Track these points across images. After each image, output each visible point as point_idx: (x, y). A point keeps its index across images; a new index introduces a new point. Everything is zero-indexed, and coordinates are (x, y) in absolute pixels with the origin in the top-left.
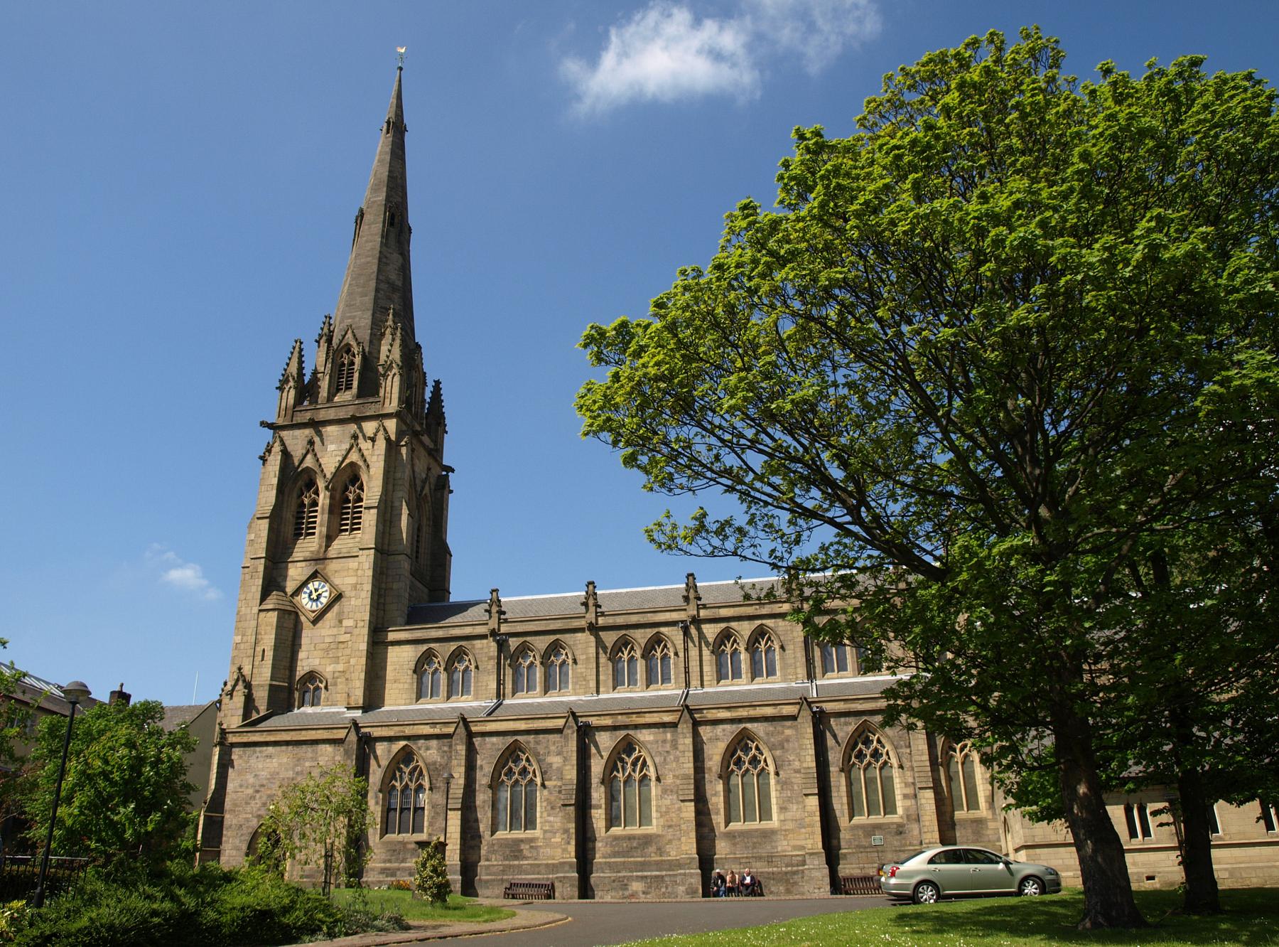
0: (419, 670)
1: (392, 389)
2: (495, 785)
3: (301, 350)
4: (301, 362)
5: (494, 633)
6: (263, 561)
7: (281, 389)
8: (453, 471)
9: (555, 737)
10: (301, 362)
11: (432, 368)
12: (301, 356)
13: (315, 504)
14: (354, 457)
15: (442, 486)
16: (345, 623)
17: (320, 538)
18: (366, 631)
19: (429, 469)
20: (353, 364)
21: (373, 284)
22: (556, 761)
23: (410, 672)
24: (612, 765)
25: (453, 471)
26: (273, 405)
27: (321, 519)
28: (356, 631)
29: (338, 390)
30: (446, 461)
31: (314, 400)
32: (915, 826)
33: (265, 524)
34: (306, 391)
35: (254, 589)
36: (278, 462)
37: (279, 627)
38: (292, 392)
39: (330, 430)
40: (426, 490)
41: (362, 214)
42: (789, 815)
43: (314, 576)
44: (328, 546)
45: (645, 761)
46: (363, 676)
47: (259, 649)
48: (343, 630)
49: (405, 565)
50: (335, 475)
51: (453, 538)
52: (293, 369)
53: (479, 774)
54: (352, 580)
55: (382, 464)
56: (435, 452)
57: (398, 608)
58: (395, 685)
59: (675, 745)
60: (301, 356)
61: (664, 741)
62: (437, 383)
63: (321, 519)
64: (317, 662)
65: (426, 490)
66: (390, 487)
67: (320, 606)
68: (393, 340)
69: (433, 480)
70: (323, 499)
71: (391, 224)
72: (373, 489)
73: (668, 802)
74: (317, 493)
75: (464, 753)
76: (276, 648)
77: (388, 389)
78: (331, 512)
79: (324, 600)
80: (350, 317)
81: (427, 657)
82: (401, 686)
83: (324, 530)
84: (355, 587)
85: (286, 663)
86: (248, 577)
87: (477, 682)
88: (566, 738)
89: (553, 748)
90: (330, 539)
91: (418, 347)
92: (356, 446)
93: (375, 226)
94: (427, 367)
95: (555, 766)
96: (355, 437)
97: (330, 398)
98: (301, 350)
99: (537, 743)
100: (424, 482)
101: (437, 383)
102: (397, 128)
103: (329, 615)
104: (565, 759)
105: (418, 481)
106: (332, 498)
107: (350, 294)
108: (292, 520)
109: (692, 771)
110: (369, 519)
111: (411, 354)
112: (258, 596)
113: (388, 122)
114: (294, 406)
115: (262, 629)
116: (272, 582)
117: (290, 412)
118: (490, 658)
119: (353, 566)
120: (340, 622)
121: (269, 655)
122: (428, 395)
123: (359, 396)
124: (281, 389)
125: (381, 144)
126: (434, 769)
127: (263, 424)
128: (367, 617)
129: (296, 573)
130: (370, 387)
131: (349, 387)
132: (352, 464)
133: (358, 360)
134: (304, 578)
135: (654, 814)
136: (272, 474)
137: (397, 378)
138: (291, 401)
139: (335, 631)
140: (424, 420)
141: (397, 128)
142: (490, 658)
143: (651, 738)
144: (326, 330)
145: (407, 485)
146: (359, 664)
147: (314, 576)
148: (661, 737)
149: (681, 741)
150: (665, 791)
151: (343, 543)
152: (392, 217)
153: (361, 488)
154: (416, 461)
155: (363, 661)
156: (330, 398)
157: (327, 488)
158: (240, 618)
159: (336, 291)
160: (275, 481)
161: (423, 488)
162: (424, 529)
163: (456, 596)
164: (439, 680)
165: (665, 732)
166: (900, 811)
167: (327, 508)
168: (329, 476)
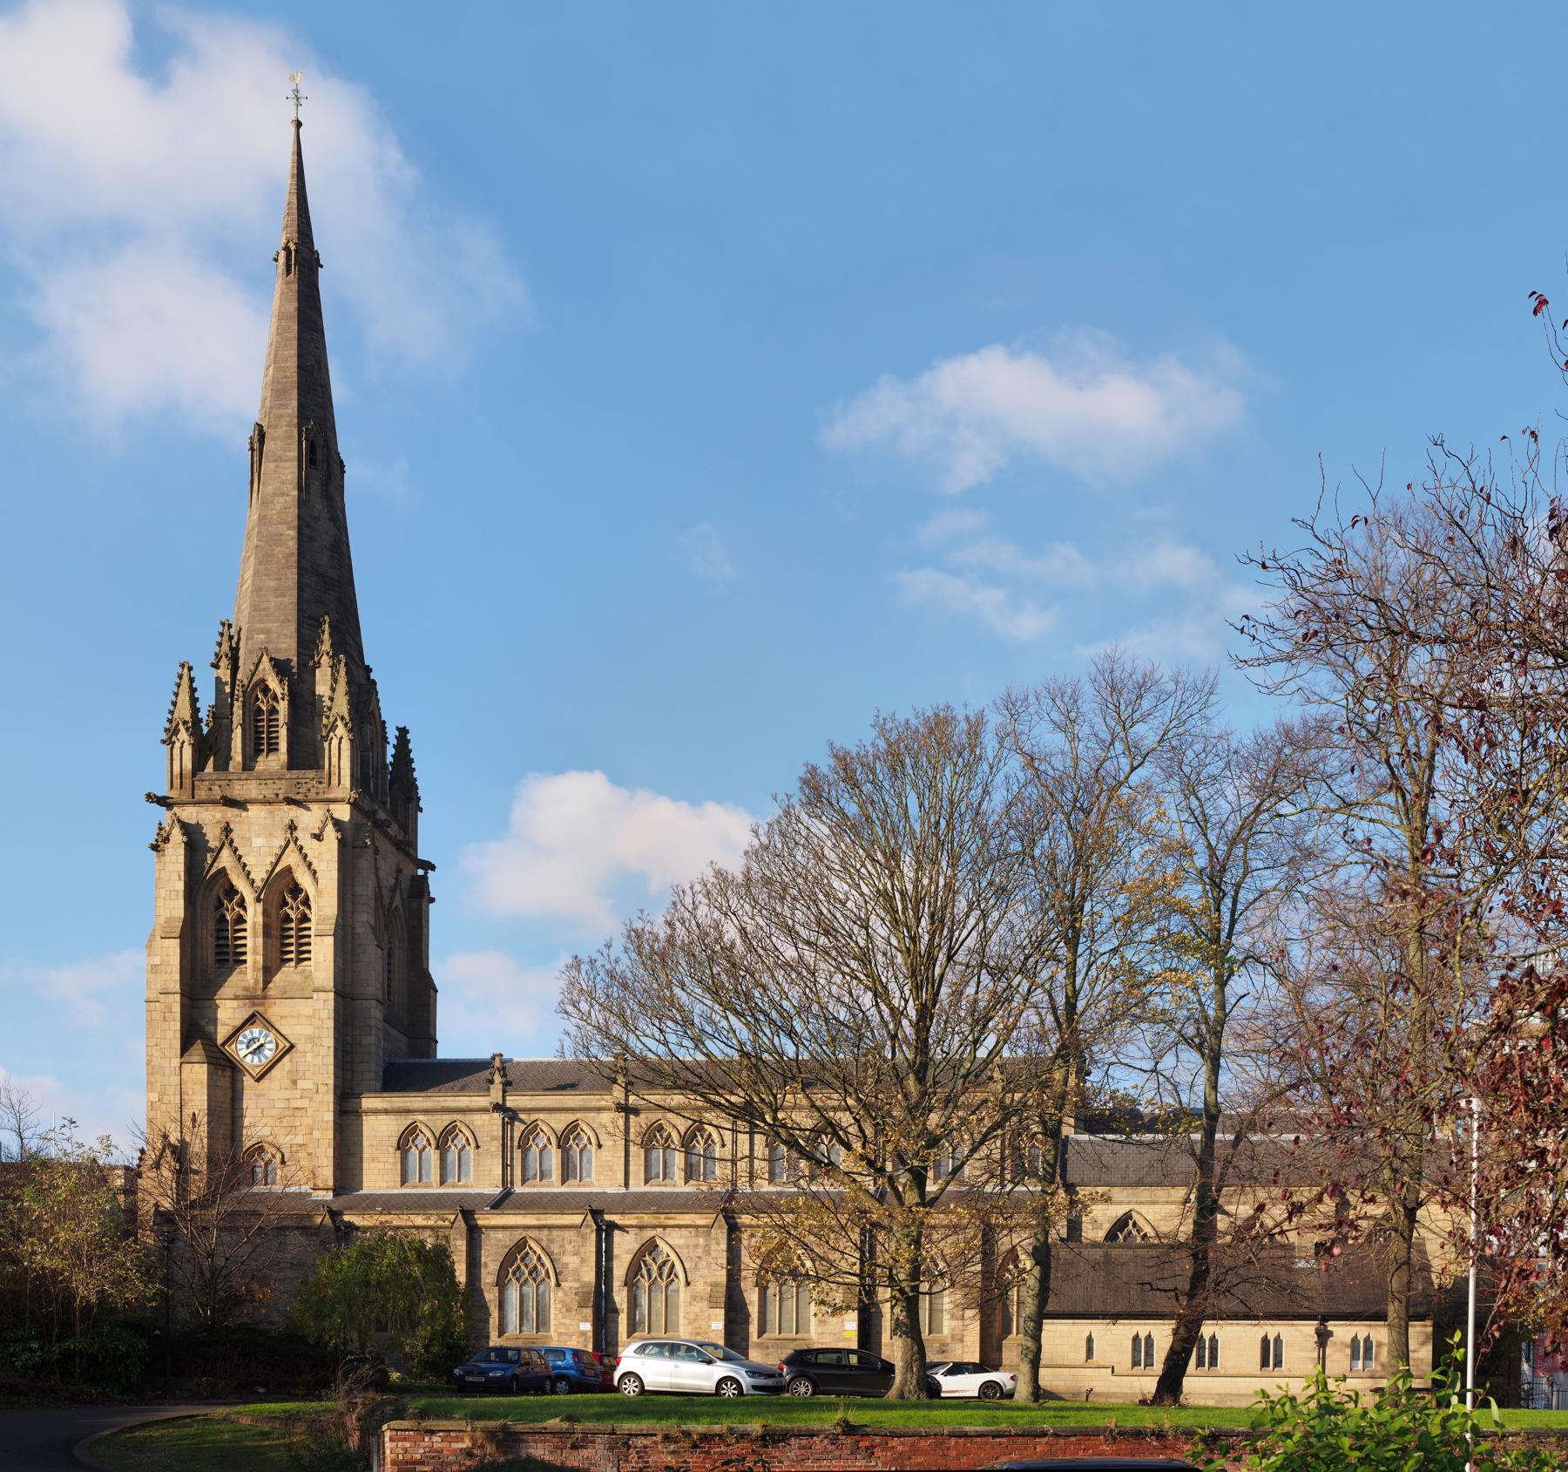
0: (403, 1145)
1: (339, 751)
2: (501, 1284)
3: (192, 680)
4: (194, 700)
5: (498, 1108)
6: (178, 997)
7: (169, 742)
8: (433, 868)
9: (570, 1234)
10: (194, 700)
11: (392, 713)
12: (193, 690)
13: (241, 920)
15: (419, 894)
16: (301, 1084)
17: (255, 969)
18: (330, 1097)
19: (399, 871)
20: (273, 711)
21: (293, 575)
22: (571, 1261)
23: (392, 1150)
24: (635, 1269)
25: (433, 868)
26: (160, 765)
27: (253, 944)
28: (317, 1098)
29: (258, 752)
30: (422, 854)
31: (223, 765)
32: (959, 1346)
33: (174, 946)
34: (209, 747)
35: (170, 1034)
36: (182, 859)
37: (212, 1086)
38: (188, 752)
40: (397, 901)
41: (261, 434)
42: (827, 1328)
43: (250, 1021)
44: (266, 982)
45: (673, 1265)
46: (331, 1152)
47: (188, 1112)
48: (298, 1093)
49: (375, 1013)
50: (266, 882)
51: (439, 968)
52: (184, 711)
53: (616, 1264)
54: (308, 1030)
55: (335, 874)
56: (407, 845)
57: (370, 1069)
58: (373, 1165)
59: (707, 1251)
60: (193, 690)
61: (696, 1246)
62: (403, 732)
63: (253, 944)
64: (267, 1131)
65: (397, 901)
66: (349, 904)
67: (247, 1033)
68: (335, 681)
69: (405, 883)
70: (254, 915)
71: (312, 462)
72: (324, 901)
73: (697, 1309)
74: (242, 904)
75: (464, 1248)
76: (211, 1112)
77: (335, 760)
78: (266, 934)
79: (269, 1053)
80: (262, 631)
81: (410, 1133)
82: (381, 1166)
83: (260, 958)
84: (311, 1039)
85: (224, 1131)
86: (156, 1016)
87: (477, 1165)
88: (584, 1237)
89: (569, 1248)
90: (269, 972)
91: (374, 682)
92: (287, 837)
93: (284, 470)
94: (385, 715)
95: (571, 1266)
97: (248, 765)
98: (192, 680)
99: (551, 1241)
100: (393, 890)
101: (403, 732)
102: (303, 261)
103: (275, 1072)
104: (583, 1260)
105: (385, 892)
106: (265, 913)
107: (257, 589)
108: (211, 942)
109: (724, 1279)
110: (323, 951)
111: (363, 692)
112: (177, 1044)
113: (287, 249)
114: (194, 774)
115: (188, 1087)
116: (196, 1030)
117: (188, 783)
118: (493, 1138)
119: (306, 1011)
120: (294, 1082)
121: (203, 1119)
122: (390, 751)
123: (292, 765)
124: (169, 742)
125: (278, 292)
127: (150, 798)
128: (331, 1082)
129: (228, 1013)
130: (306, 755)
131: (273, 748)
132: (288, 870)
133: (283, 707)
134: (238, 1023)
135: (682, 1321)
136: (175, 876)
137: (346, 745)
138: (188, 764)
139: (288, 1094)
140: (388, 792)
142: (493, 1138)
143: (682, 1242)
144: (225, 647)
145: (372, 903)
146: (324, 1138)
147: (250, 1021)
148: (693, 1241)
149: (714, 1247)
150: (694, 1298)
151: (287, 975)
152: (312, 448)
153: (306, 902)
154: (381, 863)
155: (330, 1134)
156: (248, 765)
157: (258, 900)
158: (152, 1067)
159: (234, 582)
160: (180, 886)
161: (392, 898)
162: (397, 953)
163: (448, 1048)
164: (429, 1161)
165: (697, 1236)
166: (946, 1331)
167: (260, 929)
168: (259, 883)
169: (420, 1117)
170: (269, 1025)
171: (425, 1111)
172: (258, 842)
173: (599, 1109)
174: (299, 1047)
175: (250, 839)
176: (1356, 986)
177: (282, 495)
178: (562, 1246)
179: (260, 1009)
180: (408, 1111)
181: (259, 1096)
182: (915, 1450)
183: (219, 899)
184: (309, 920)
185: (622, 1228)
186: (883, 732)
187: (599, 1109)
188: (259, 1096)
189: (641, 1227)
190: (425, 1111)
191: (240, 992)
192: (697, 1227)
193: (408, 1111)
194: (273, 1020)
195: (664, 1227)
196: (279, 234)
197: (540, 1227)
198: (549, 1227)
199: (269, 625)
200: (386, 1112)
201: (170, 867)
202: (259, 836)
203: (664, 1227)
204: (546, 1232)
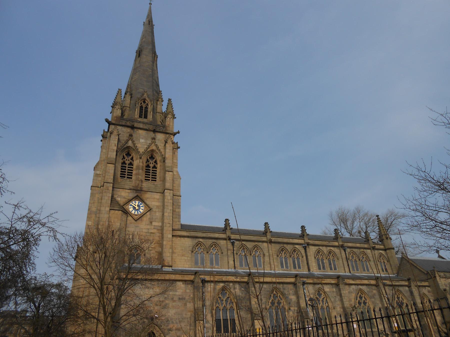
14: (153, 147)
16: (154, 224)
20: (146, 108)
39: (140, 132)
82: (186, 258)
96: (154, 139)
102: (149, 23)
120: (151, 223)
136: (113, 145)
139: (149, 227)
141: (149, 23)
169: (201, 240)
170: (142, 200)
171: (203, 238)
173: (263, 242)
174: (154, 210)
175: (139, 139)
176: (282, 250)
178: (288, 291)
179: (139, 194)
180: (197, 237)
181: (137, 226)
183: (124, 156)
184: (156, 168)
188: (137, 226)
190: (203, 238)
192: (332, 284)
193: (197, 237)
194: (144, 199)
196: (144, 19)
197: (279, 283)
198: (283, 283)
200: (188, 237)
201: (112, 141)
202: (142, 139)
204: (281, 285)
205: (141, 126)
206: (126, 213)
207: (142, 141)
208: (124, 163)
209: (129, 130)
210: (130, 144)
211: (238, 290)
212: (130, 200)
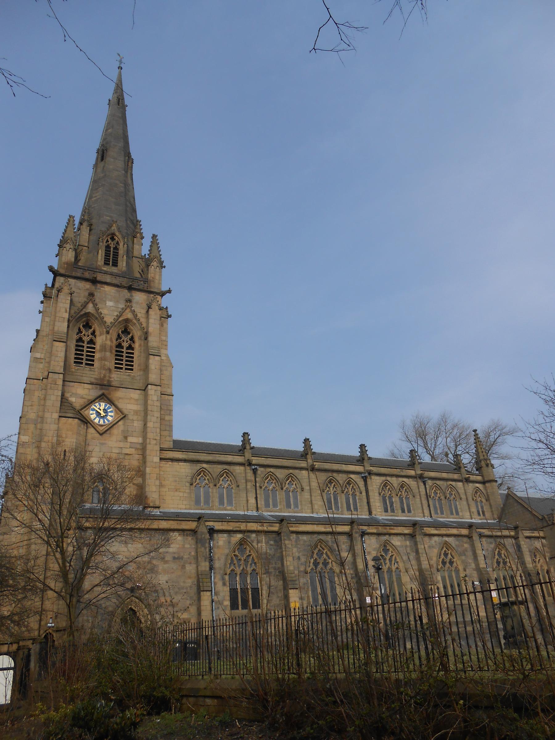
14: (129, 316)
16: (130, 439)
48: (128, 445)
82: (181, 494)
96: (129, 301)
102: (119, 103)
120: (126, 438)
126: (266, 559)
136: (64, 310)
139: (122, 445)
141: (119, 103)
165: (405, 540)
170: (111, 402)
171: (208, 462)
172: (110, 304)
173: (301, 469)
174: (130, 417)
175: (105, 301)
177: (117, 171)
179: (105, 392)
180: (198, 461)
181: (102, 444)
182: (448, 628)
184: (133, 349)
185: (368, 534)
186: (498, 420)
187: (301, 469)
189: (379, 534)
190: (208, 462)
191: (93, 380)
192: (405, 535)
193: (198, 461)
194: (114, 399)
195: (390, 534)
199: (112, 215)
200: (185, 461)
202: (111, 301)
203: (390, 534)
205: (108, 279)
206: (86, 421)
207: (110, 304)
208: (80, 340)
209: (88, 285)
210: (90, 308)
211: (263, 545)
212: (92, 402)
